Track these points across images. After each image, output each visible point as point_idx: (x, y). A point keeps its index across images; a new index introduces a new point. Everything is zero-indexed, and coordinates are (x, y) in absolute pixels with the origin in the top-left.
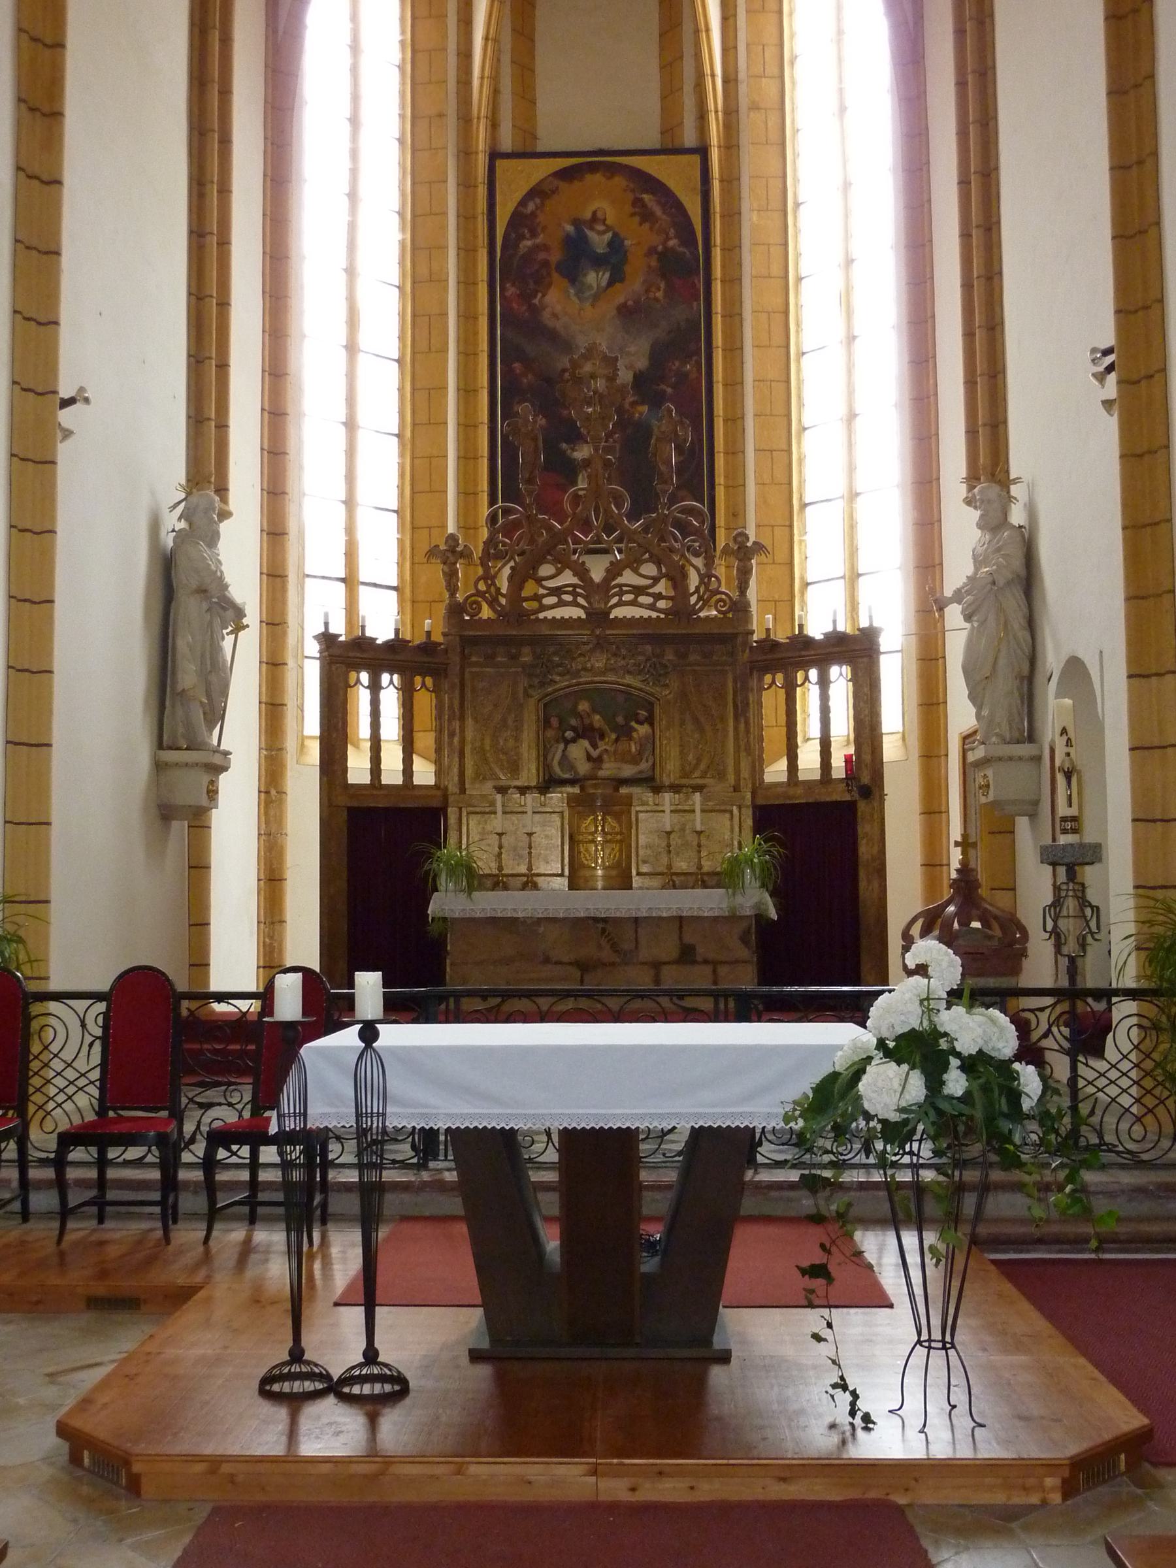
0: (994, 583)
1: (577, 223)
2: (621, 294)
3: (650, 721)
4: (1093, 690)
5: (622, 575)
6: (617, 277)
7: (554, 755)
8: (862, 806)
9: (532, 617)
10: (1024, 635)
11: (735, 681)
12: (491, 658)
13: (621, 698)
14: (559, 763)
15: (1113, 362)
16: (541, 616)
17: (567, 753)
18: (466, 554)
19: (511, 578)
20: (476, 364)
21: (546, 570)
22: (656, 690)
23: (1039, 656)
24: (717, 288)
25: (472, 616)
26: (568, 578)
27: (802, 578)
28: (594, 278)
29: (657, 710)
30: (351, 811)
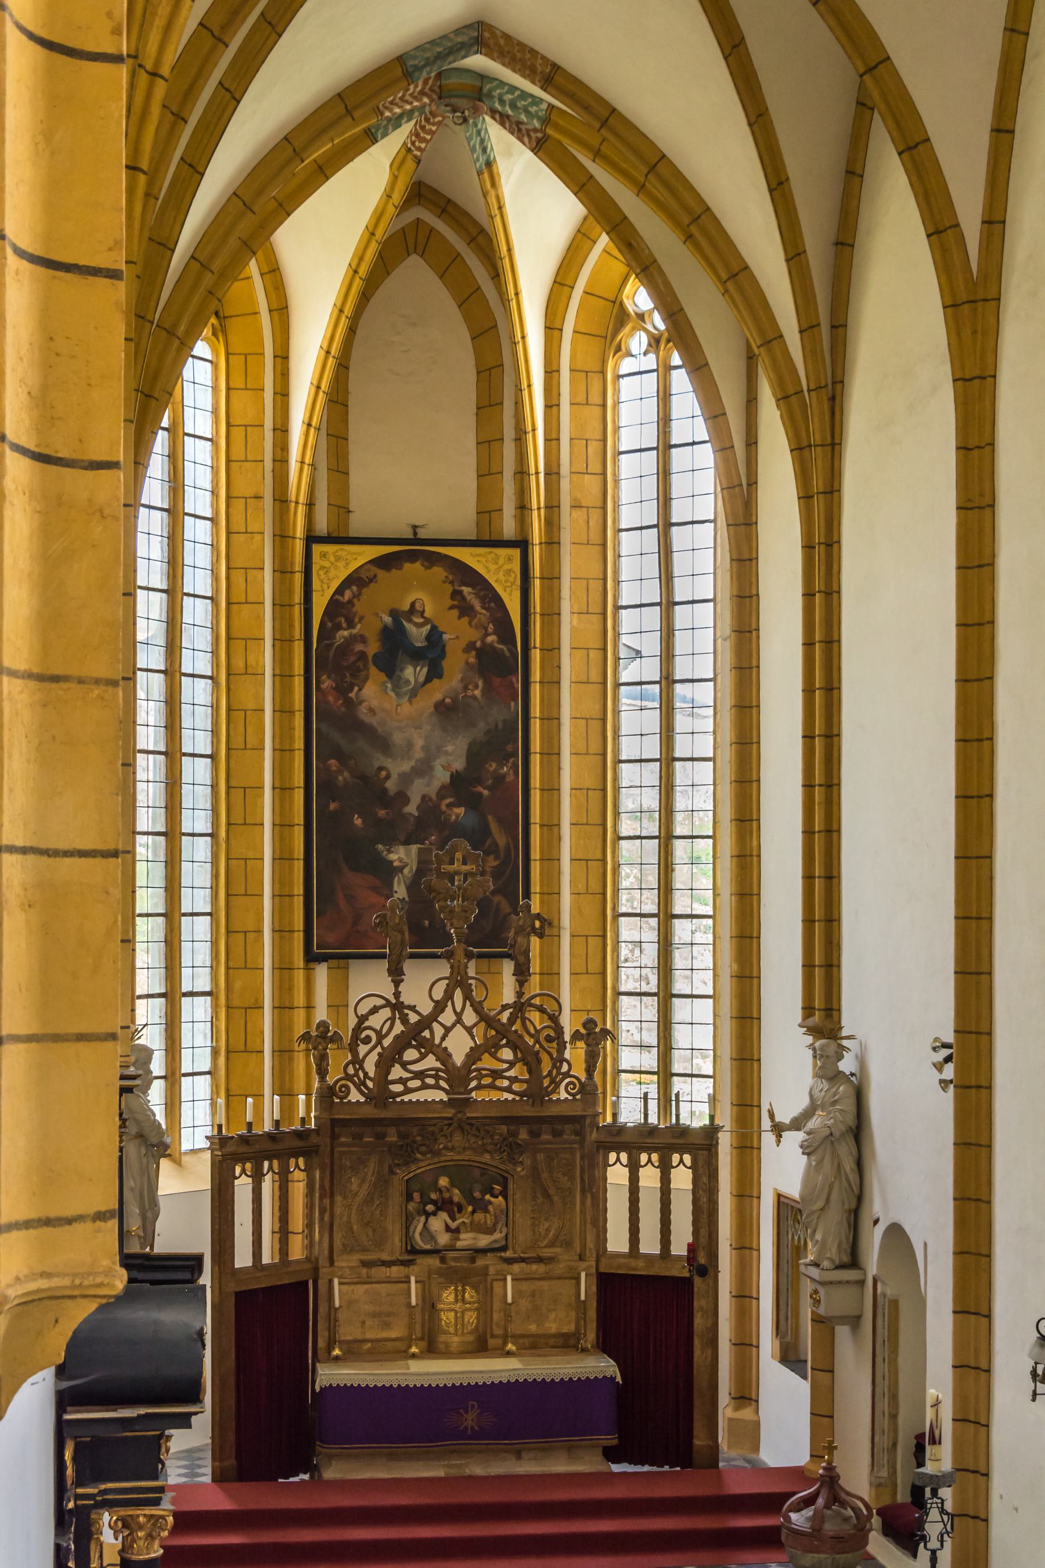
0: (831, 1134)
1: (394, 614)
2: (438, 691)
3: (504, 1194)
4: (918, 1269)
5: (481, 1060)
6: (435, 673)
7: (416, 1227)
8: (698, 1281)
9: (398, 1099)
10: (853, 1177)
11: (582, 1158)
12: (358, 1137)
13: (477, 1173)
14: (421, 1234)
15: (952, 1054)
16: (406, 1098)
17: (427, 1225)
18: (336, 1038)
19: (378, 1065)
20: (292, 760)
21: (411, 1054)
22: (509, 1167)
23: (866, 1193)
24: (536, 691)
25: (341, 1098)
26: (431, 1062)
27: (615, 988)
28: (412, 673)
29: (511, 1185)
30: (238, 1294)
